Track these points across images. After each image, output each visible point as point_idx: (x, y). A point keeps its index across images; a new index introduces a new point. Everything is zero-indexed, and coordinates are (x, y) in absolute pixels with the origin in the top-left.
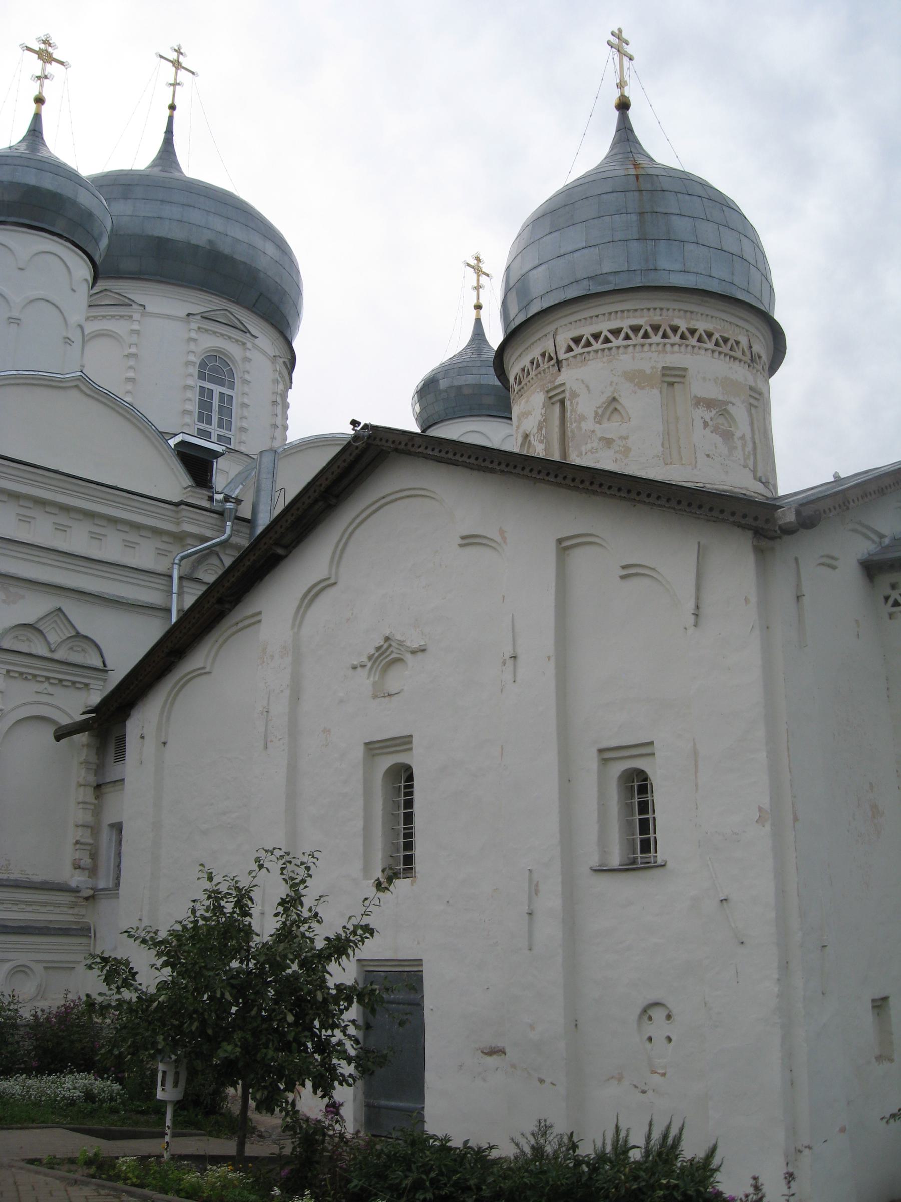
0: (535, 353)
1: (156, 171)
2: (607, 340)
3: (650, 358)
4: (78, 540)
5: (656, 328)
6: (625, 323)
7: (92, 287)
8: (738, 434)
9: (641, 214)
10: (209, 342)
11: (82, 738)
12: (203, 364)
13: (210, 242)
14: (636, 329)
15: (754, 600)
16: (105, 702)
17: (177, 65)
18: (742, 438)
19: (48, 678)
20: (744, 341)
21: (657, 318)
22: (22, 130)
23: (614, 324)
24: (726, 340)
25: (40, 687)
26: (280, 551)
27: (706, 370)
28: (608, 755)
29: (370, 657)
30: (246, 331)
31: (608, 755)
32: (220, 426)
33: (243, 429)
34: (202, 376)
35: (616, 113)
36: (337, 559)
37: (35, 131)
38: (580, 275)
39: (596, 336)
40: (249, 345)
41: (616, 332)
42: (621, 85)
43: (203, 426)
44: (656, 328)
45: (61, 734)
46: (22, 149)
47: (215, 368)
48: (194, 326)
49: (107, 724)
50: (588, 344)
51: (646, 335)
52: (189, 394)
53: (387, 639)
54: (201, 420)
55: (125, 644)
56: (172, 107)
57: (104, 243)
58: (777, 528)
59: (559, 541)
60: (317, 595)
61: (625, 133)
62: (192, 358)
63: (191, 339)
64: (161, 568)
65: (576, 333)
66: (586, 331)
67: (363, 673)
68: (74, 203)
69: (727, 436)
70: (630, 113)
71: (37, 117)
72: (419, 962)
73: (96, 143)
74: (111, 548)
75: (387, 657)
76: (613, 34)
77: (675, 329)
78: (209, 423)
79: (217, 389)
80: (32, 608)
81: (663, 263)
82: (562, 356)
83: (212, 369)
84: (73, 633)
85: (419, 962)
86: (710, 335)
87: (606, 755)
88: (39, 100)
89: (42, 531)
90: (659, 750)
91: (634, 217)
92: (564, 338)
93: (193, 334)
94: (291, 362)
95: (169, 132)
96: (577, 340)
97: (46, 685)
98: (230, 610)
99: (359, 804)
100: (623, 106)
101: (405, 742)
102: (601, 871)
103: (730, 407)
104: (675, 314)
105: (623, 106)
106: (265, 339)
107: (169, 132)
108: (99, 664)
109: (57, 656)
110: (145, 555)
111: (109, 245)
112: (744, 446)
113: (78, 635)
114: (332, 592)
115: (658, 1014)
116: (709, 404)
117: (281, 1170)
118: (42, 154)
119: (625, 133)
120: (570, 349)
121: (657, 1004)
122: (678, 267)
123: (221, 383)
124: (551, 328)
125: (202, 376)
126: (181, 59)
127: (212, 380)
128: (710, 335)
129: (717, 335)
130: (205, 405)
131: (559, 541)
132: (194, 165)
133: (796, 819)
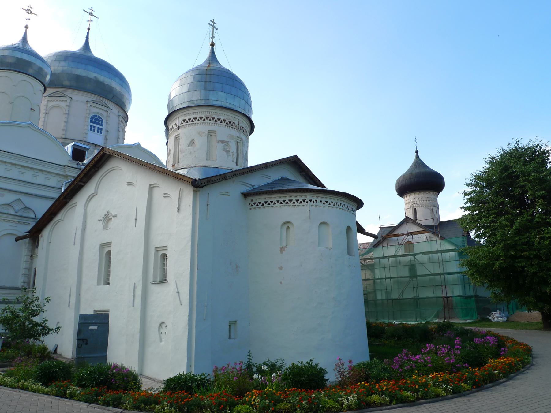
0: (173, 124)
1: (83, 52)
2: (193, 121)
3: (205, 127)
4: (28, 176)
5: (207, 118)
6: (192, 117)
7: (45, 92)
8: (231, 151)
9: (206, 82)
10: (96, 110)
11: (27, 240)
12: (92, 118)
13: (95, 77)
14: (201, 118)
15: (191, 205)
16: (32, 229)
17: (91, 14)
18: (233, 152)
19: (14, 221)
20: (237, 123)
21: (208, 115)
22: (20, 37)
23: (195, 116)
24: (230, 122)
25: (11, 224)
26: (82, 184)
27: (223, 132)
28: (158, 249)
29: (103, 218)
30: (108, 107)
31: (158, 249)
34: (91, 122)
36: (97, 188)
37: (25, 39)
38: (186, 100)
39: (189, 120)
40: (109, 112)
41: (195, 119)
42: (213, 38)
44: (207, 118)
45: (17, 239)
46: (20, 45)
48: (89, 105)
49: (34, 235)
50: (187, 122)
51: (204, 120)
53: (108, 212)
55: (41, 208)
56: (89, 29)
57: (48, 78)
59: (150, 185)
60: (92, 198)
64: (59, 186)
65: (184, 118)
66: (187, 118)
67: (101, 222)
68: (35, 64)
69: (228, 152)
70: (214, 47)
72: (108, 311)
73: (48, 44)
74: (40, 179)
75: (107, 218)
76: (211, 21)
77: (213, 118)
79: (97, 126)
80: (9, 198)
81: (211, 98)
82: (180, 125)
84: (24, 207)
85: (108, 311)
86: (225, 121)
87: (157, 249)
88: (27, 27)
89: (14, 173)
90: (169, 248)
91: (203, 83)
92: (181, 120)
94: (126, 119)
96: (184, 121)
97: (14, 223)
98: (69, 201)
99: (97, 263)
101: (109, 244)
102: (154, 283)
103: (229, 143)
104: (214, 113)
106: (115, 110)
108: (34, 217)
109: (17, 214)
110: (53, 182)
111: (50, 79)
112: (233, 155)
113: (26, 207)
114: (96, 197)
115: (164, 326)
116: (222, 142)
118: (27, 47)
120: (182, 123)
121: (163, 323)
122: (216, 99)
124: (177, 116)
125: (91, 122)
126: (93, 12)
127: (95, 123)
128: (225, 121)
129: (227, 121)
131: (150, 185)
132: (98, 51)
133: (198, 269)
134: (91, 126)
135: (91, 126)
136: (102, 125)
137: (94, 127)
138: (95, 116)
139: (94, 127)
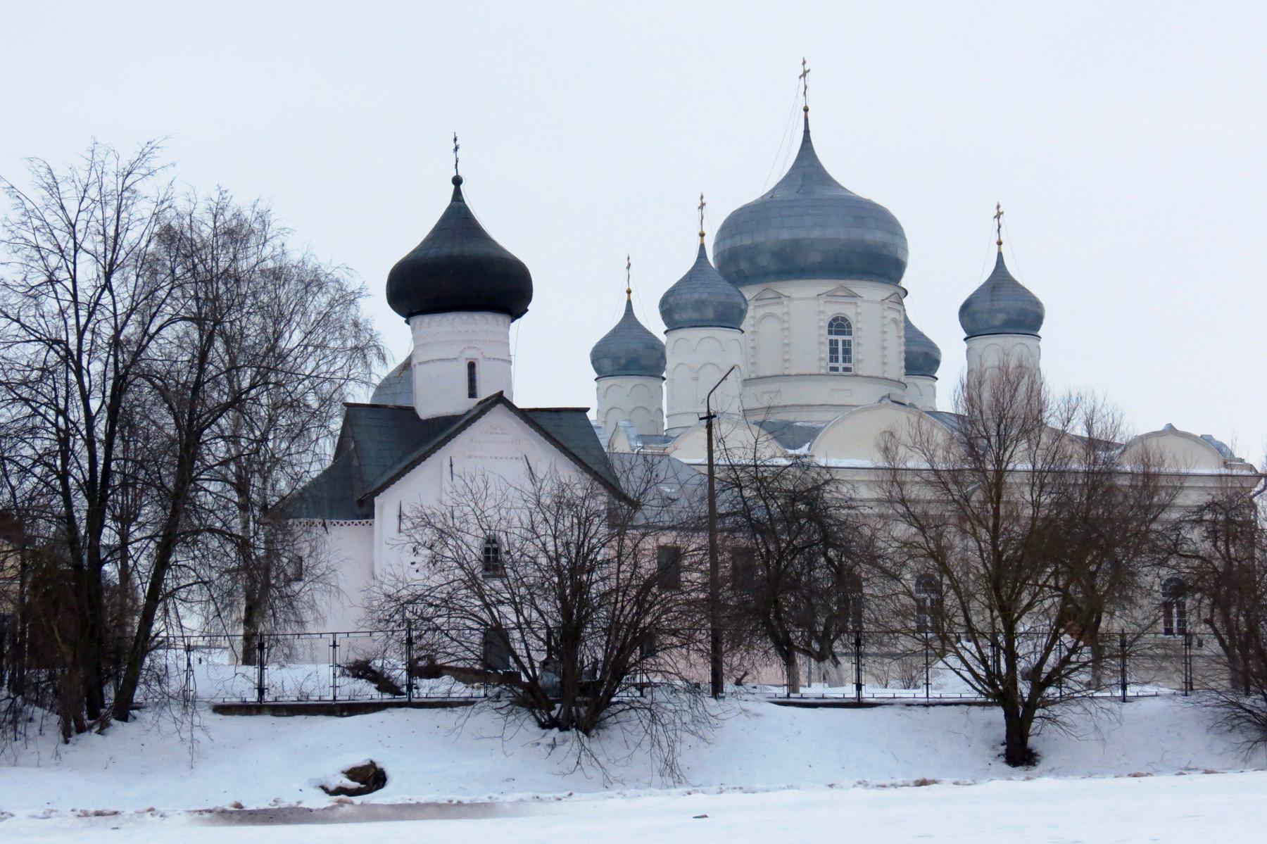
10: (833, 310)
12: (830, 325)
30: (855, 296)
32: (844, 361)
33: (858, 361)
34: (830, 333)
35: (453, 187)
43: (834, 365)
47: (839, 326)
52: (823, 347)
54: (831, 361)
58: (396, 336)
61: (457, 195)
62: (822, 324)
63: (820, 312)
71: (1000, 255)
78: (837, 361)
79: (840, 338)
83: (837, 326)
93: (822, 309)
95: (807, 132)
100: (457, 181)
105: (457, 181)
107: (807, 132)
117: (503, 576)
119: (457, 195)
123: (843, 333)
125: (830, 333)
127: (837, 333)
130: (833, 351)
132: (851, 172)
134: (831, 341)
135: (831, 341)
136: (850, 333)
137: (837, 341)
138: (835, 319)
139: (837, 341)
